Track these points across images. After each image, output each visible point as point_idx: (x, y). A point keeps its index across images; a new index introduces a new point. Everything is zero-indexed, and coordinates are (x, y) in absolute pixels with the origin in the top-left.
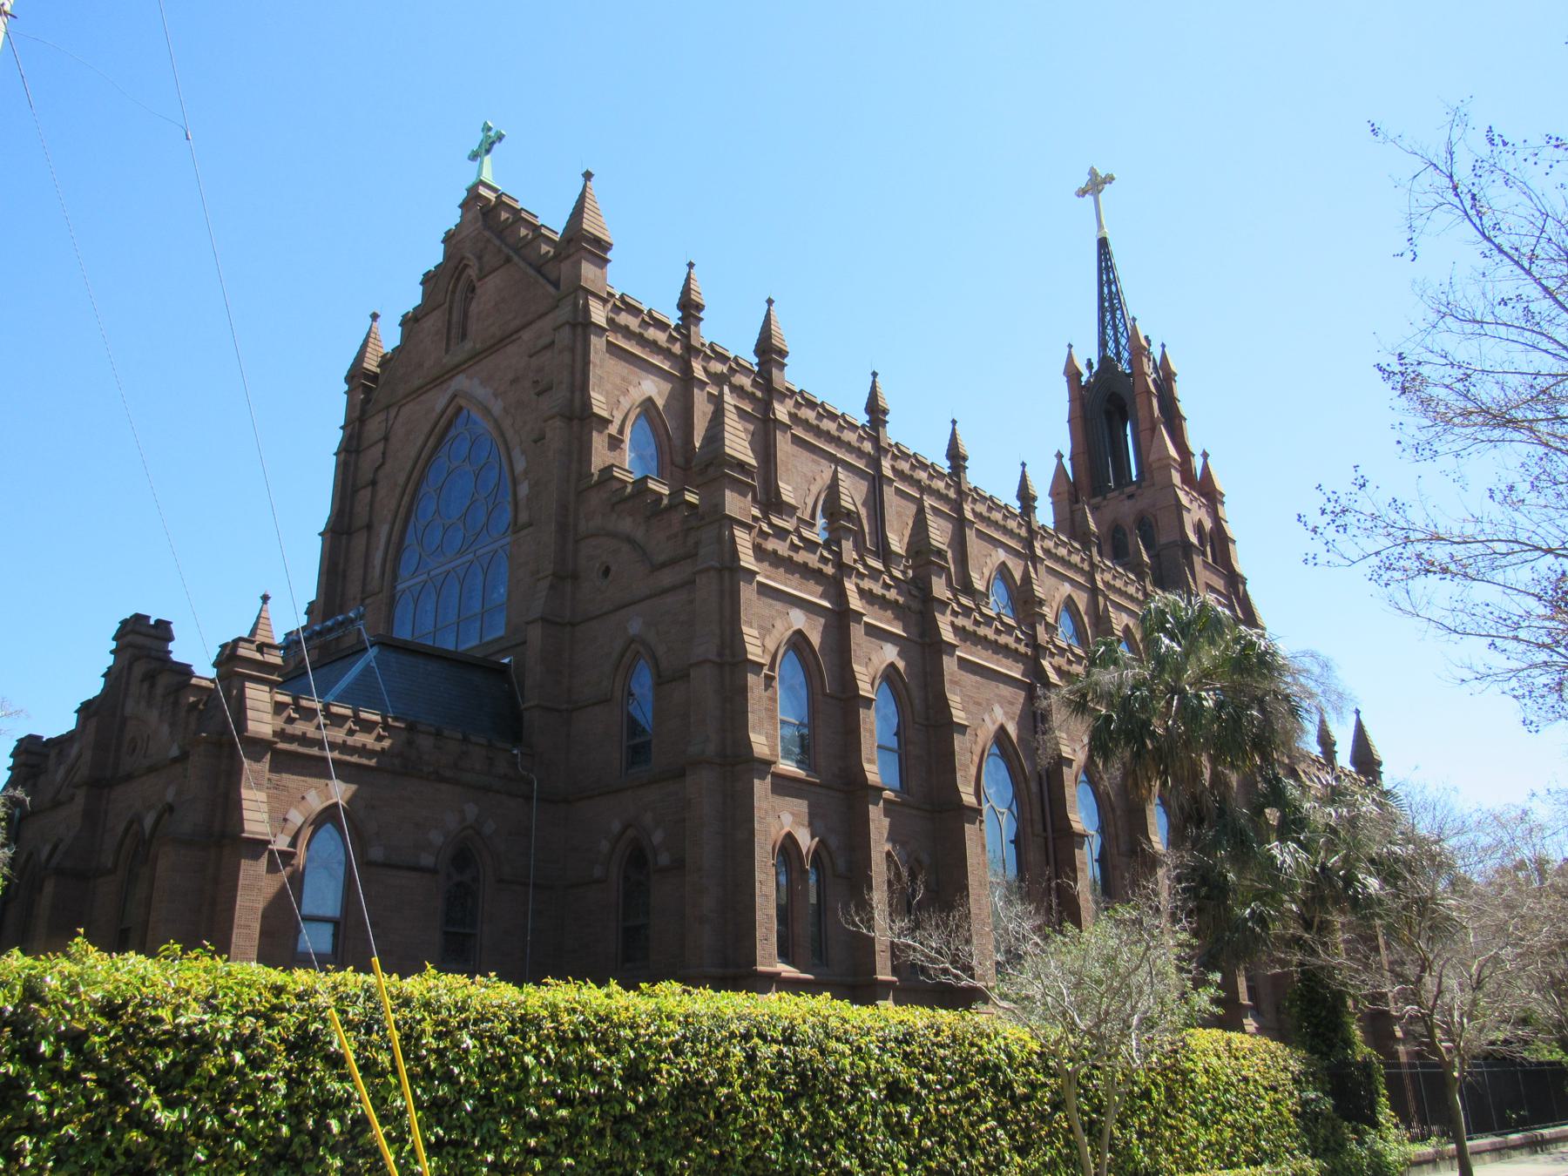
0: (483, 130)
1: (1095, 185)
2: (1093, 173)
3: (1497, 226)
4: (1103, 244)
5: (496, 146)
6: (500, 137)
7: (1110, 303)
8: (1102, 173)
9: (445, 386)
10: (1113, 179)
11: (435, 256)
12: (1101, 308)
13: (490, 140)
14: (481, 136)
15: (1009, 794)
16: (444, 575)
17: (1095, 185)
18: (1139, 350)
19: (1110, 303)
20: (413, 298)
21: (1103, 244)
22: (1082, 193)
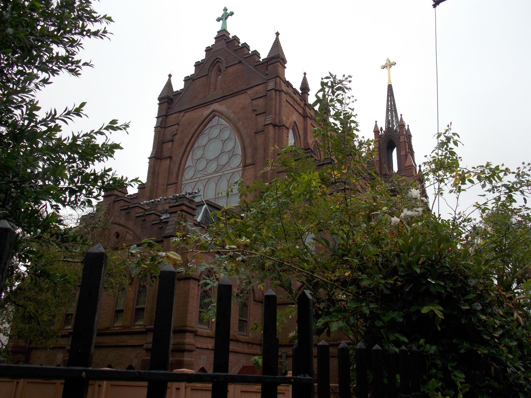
0: (224, 10)
1: (389, 65)
2: (225, 10)
3: (349, 79)
4: (390, 88)
5: (230, 17)
6: (232, 14)
7: (391, 108)
8: (392, 61)
9: (208, 107)
10: (395, 64)
11: (202, 56)
12: (388, 111)
13: (227, 15)
14: (223, 12)
15: (168, 391)
16: (193, 178)
17: (389, 65)
18: (402, 125)
19: (391, 108)
20: (191, 71)
21: (390, 88)
22: (383, 67)
